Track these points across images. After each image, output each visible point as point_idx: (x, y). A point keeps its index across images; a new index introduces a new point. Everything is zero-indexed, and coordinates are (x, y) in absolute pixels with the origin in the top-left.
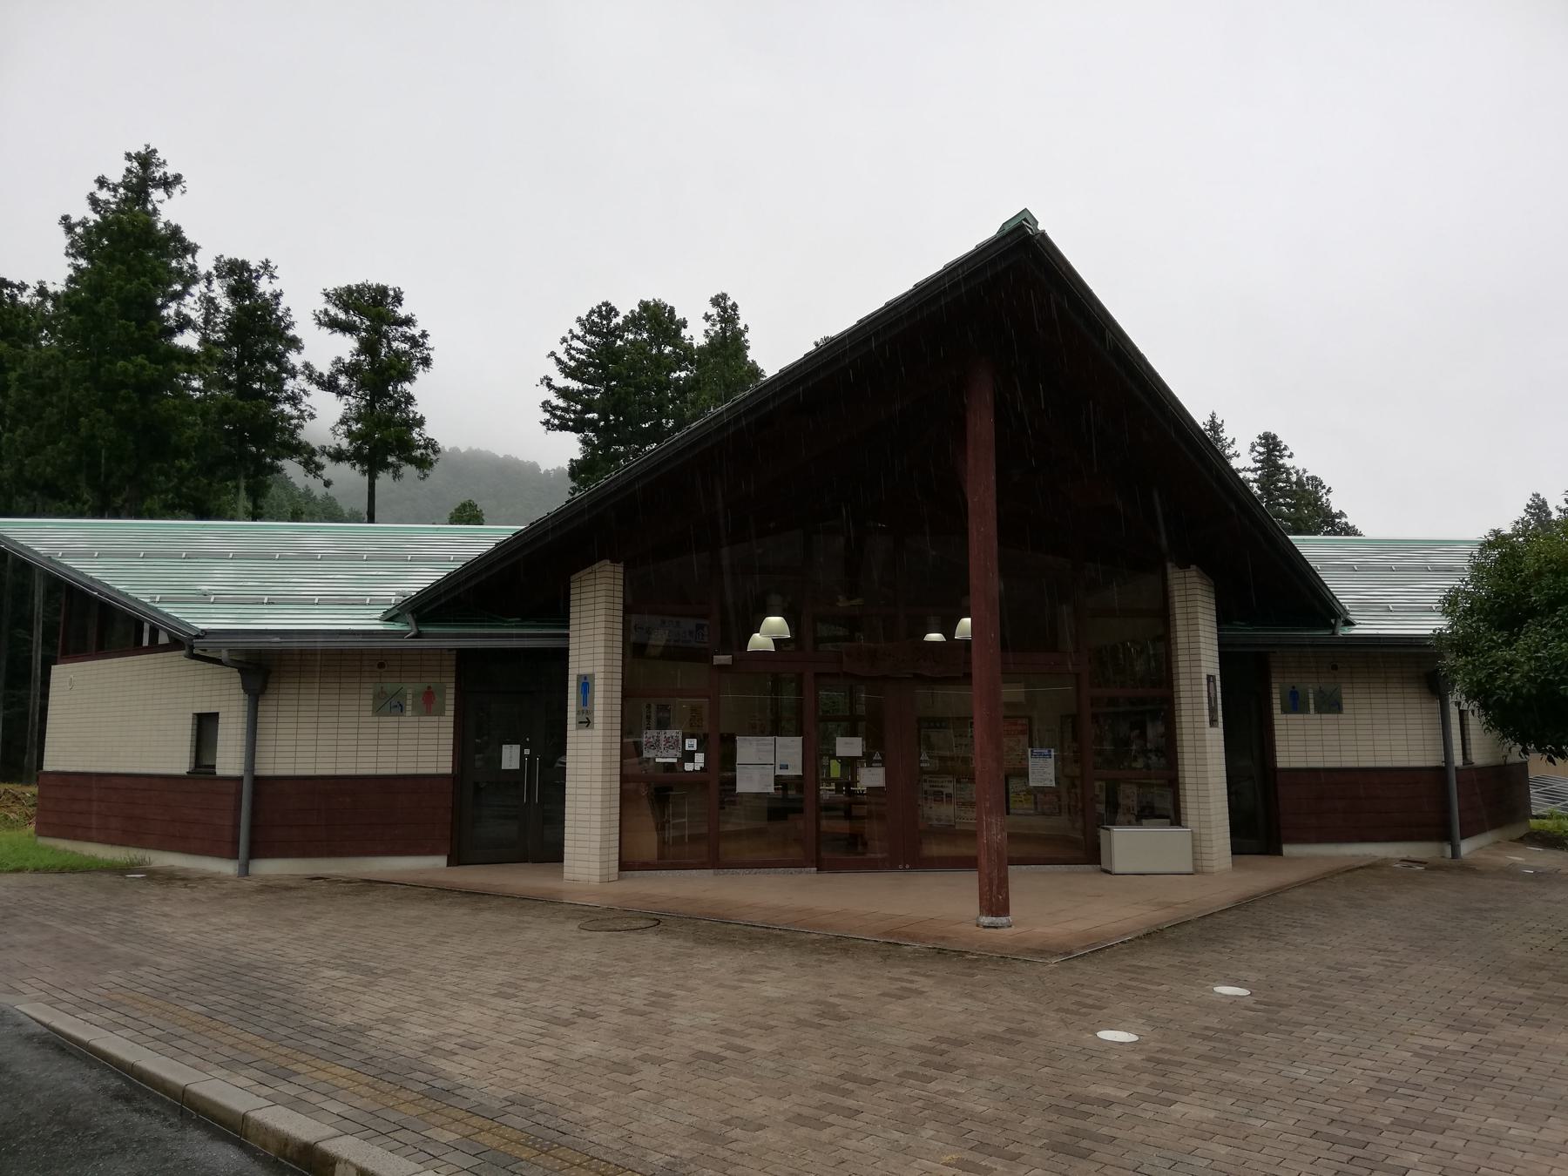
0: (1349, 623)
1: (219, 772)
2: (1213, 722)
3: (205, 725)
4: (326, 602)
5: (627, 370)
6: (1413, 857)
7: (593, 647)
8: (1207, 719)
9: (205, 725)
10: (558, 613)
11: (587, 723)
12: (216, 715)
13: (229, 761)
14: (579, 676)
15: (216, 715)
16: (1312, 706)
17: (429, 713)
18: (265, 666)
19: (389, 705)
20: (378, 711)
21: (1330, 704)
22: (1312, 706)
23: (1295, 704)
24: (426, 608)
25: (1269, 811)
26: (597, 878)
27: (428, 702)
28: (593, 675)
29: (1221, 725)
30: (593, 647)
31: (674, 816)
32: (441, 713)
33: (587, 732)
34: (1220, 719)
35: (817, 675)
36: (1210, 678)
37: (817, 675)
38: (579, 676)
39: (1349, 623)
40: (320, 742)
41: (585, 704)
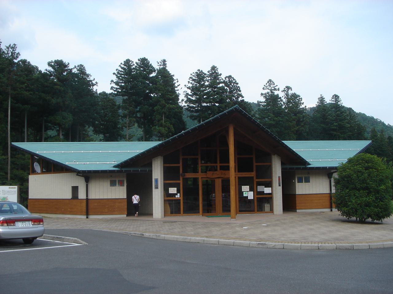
0: (310, 164)
1: (79, 198)
2: (280, 185)
3: (75, 190)
4: (26, 144)
5: (124, 62)
6: (321, 211)
7: (157, 173)
8: (278, 185)
9: (75, 190)
10: (150, 165)
11: (157, 187)
12: (78, 186)
13: (82, 195)
14: (155, 179)
15: (78, 186)
16: (304, 181)
17: (121, 186)
18: (89, 176)
19: (113, 184)
20: (111, 186)
21: (307, 181)
22: (304, 181)
23: (300, 181)
24: (124, 165)
25: (290, 203)
26: (160, 217)
27: (121, 184)
28: (158, 179)
29: (281, 186)
30: (157, 173)
31: (173, 207)
32: (124, 186)
33: (157, 190)
34: (281, 185)
35: (202, 178)
36: (279, 177)
37: (202, 178)
38: (155, 179)
39: (310, 164)
40: (101, 191)
41: (156, 184)
